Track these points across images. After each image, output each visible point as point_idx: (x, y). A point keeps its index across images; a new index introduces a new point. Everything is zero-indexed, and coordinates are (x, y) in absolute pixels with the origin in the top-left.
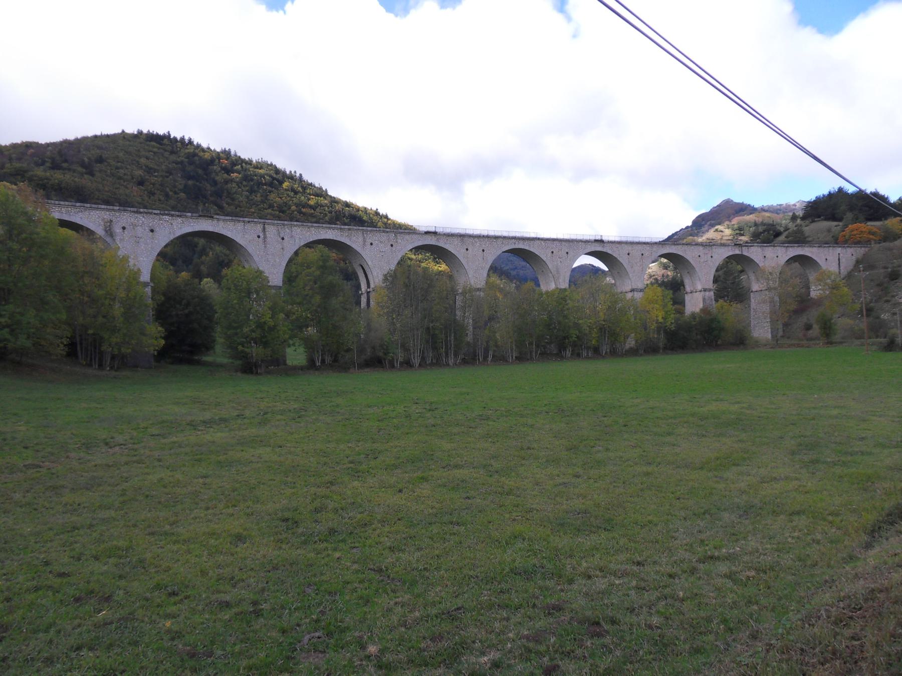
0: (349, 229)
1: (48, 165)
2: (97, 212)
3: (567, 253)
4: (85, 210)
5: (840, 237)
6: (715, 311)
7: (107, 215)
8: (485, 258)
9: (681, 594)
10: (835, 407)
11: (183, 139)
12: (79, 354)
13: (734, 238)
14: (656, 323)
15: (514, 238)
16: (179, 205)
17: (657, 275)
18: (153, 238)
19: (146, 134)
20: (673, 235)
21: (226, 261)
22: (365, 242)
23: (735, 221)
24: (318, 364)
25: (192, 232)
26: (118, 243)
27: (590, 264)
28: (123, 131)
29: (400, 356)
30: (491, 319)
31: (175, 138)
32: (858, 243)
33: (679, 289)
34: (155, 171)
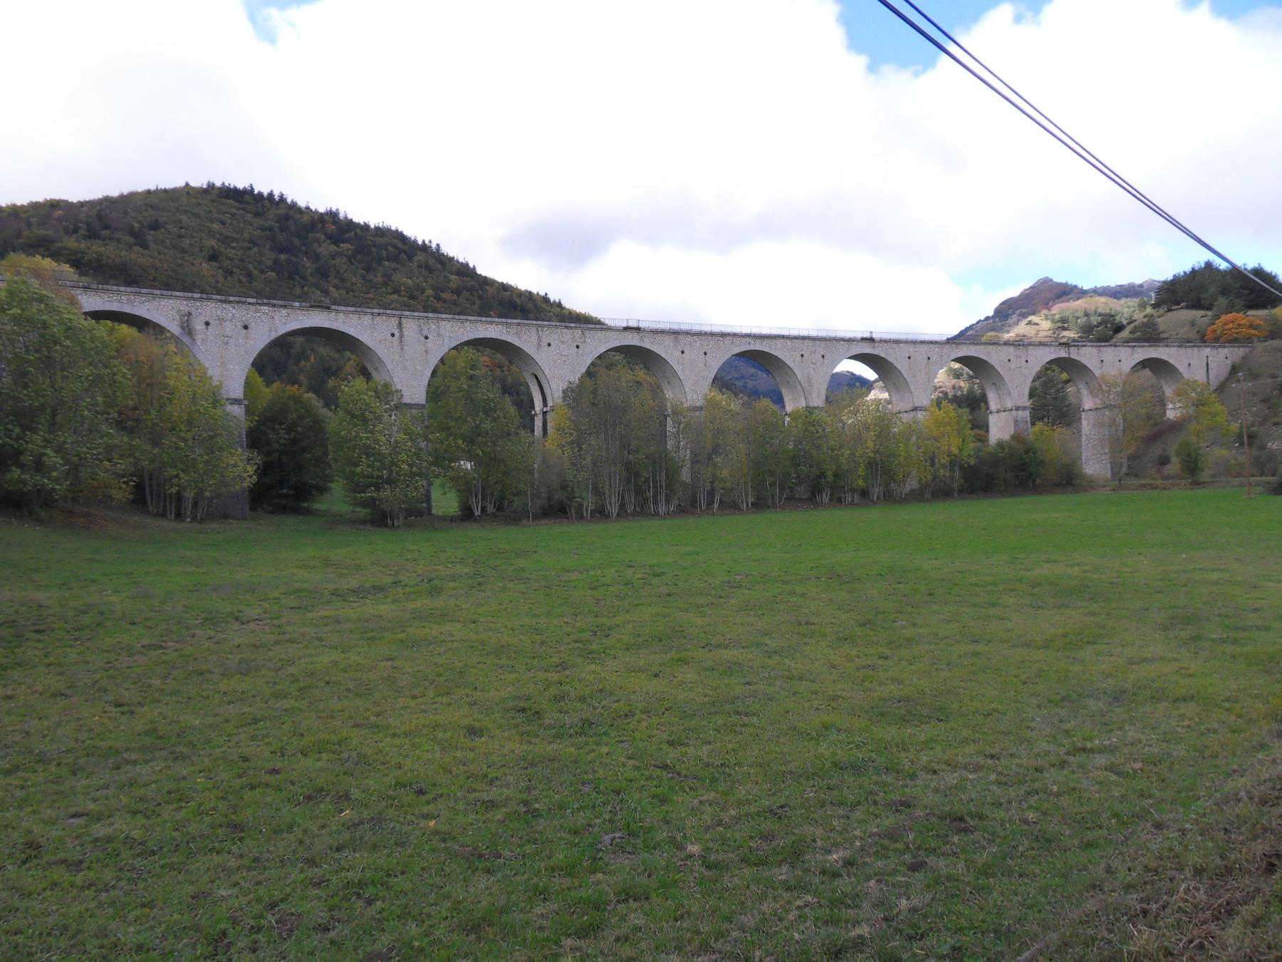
0: (519, 324)
1: (82, 232)
2: (171, 301)
3: (823, 356)
4: (154, 299)
5: (1208, 333)
6: (1031, 438)
7: (184, 306)
8: (707, 364)
9: (1055, 788)
10: (1213, 571)
11: (271, 195)
12: (149, 498)
13: (1054, 333)
14: (948, 456)
15: (749, 336)
16: (267, 289)
17: (945, 387)
18: (247, 338)
19: (219, 189)
20: (967, 329)
21: (334, 368)
22: (540, 340)
23: (1058, 309)
24: (477, 513)
25: (302, 329)
26: (199, 344)
27: (848, 372)
28: (187, 184)
29: (589, 502)
30: (716, 449)
31: (260, 194)
32: (1234, 341)
33: (979, 407)
34: (234, 240)
